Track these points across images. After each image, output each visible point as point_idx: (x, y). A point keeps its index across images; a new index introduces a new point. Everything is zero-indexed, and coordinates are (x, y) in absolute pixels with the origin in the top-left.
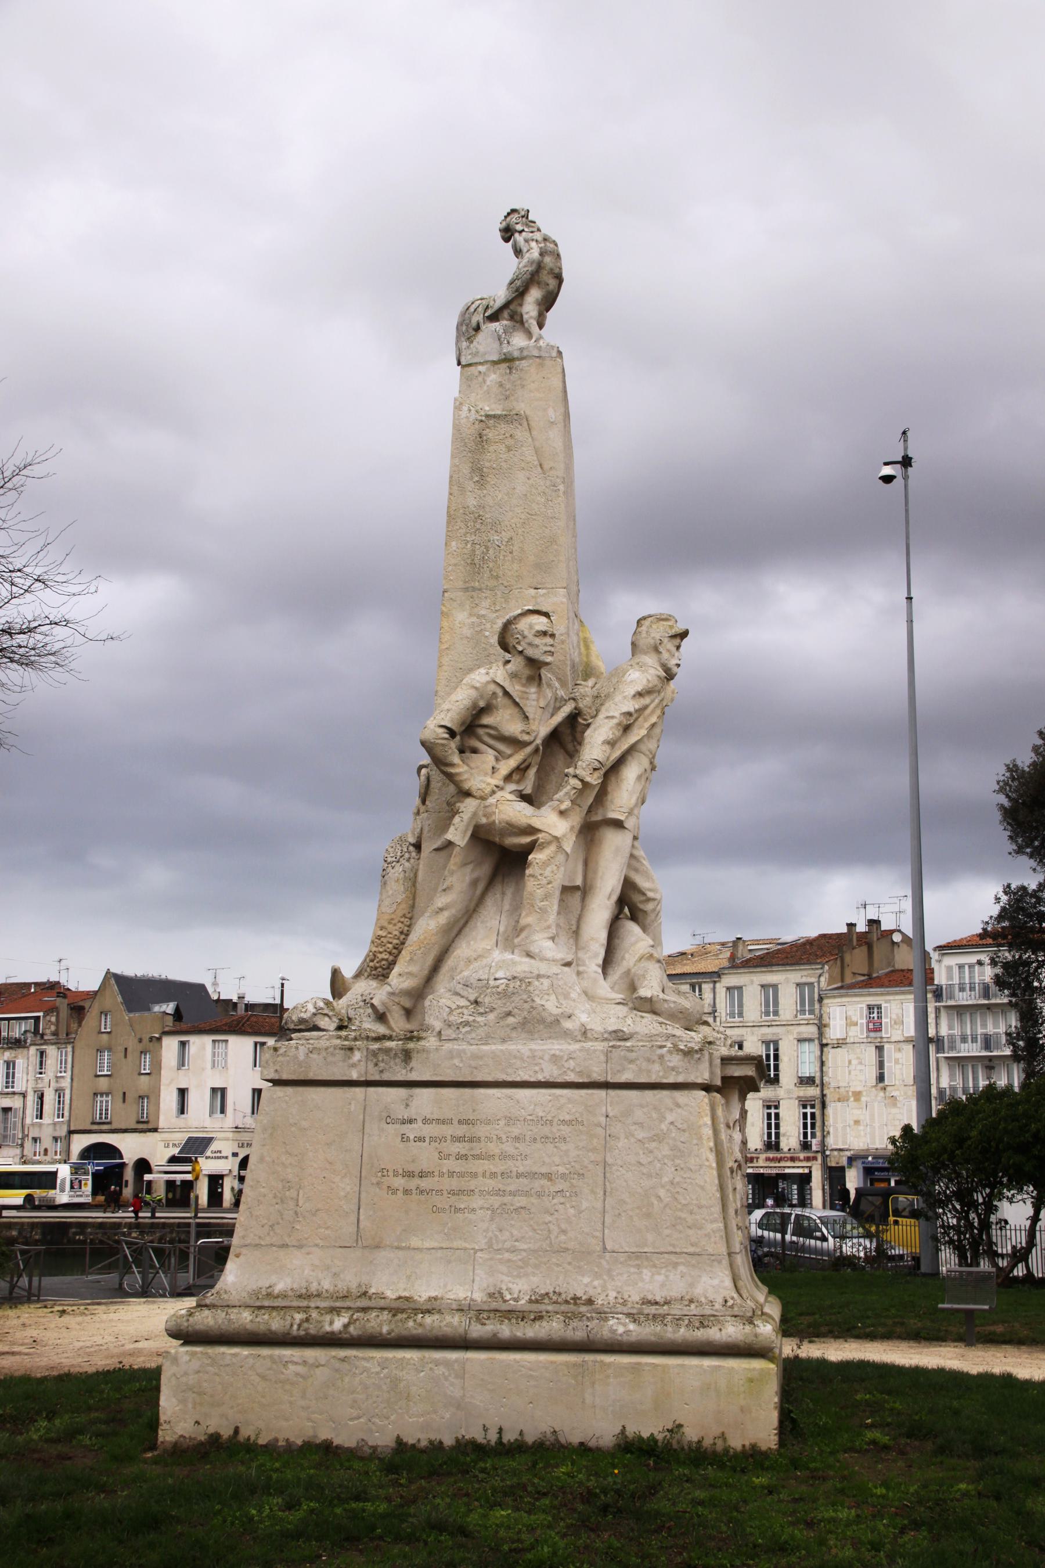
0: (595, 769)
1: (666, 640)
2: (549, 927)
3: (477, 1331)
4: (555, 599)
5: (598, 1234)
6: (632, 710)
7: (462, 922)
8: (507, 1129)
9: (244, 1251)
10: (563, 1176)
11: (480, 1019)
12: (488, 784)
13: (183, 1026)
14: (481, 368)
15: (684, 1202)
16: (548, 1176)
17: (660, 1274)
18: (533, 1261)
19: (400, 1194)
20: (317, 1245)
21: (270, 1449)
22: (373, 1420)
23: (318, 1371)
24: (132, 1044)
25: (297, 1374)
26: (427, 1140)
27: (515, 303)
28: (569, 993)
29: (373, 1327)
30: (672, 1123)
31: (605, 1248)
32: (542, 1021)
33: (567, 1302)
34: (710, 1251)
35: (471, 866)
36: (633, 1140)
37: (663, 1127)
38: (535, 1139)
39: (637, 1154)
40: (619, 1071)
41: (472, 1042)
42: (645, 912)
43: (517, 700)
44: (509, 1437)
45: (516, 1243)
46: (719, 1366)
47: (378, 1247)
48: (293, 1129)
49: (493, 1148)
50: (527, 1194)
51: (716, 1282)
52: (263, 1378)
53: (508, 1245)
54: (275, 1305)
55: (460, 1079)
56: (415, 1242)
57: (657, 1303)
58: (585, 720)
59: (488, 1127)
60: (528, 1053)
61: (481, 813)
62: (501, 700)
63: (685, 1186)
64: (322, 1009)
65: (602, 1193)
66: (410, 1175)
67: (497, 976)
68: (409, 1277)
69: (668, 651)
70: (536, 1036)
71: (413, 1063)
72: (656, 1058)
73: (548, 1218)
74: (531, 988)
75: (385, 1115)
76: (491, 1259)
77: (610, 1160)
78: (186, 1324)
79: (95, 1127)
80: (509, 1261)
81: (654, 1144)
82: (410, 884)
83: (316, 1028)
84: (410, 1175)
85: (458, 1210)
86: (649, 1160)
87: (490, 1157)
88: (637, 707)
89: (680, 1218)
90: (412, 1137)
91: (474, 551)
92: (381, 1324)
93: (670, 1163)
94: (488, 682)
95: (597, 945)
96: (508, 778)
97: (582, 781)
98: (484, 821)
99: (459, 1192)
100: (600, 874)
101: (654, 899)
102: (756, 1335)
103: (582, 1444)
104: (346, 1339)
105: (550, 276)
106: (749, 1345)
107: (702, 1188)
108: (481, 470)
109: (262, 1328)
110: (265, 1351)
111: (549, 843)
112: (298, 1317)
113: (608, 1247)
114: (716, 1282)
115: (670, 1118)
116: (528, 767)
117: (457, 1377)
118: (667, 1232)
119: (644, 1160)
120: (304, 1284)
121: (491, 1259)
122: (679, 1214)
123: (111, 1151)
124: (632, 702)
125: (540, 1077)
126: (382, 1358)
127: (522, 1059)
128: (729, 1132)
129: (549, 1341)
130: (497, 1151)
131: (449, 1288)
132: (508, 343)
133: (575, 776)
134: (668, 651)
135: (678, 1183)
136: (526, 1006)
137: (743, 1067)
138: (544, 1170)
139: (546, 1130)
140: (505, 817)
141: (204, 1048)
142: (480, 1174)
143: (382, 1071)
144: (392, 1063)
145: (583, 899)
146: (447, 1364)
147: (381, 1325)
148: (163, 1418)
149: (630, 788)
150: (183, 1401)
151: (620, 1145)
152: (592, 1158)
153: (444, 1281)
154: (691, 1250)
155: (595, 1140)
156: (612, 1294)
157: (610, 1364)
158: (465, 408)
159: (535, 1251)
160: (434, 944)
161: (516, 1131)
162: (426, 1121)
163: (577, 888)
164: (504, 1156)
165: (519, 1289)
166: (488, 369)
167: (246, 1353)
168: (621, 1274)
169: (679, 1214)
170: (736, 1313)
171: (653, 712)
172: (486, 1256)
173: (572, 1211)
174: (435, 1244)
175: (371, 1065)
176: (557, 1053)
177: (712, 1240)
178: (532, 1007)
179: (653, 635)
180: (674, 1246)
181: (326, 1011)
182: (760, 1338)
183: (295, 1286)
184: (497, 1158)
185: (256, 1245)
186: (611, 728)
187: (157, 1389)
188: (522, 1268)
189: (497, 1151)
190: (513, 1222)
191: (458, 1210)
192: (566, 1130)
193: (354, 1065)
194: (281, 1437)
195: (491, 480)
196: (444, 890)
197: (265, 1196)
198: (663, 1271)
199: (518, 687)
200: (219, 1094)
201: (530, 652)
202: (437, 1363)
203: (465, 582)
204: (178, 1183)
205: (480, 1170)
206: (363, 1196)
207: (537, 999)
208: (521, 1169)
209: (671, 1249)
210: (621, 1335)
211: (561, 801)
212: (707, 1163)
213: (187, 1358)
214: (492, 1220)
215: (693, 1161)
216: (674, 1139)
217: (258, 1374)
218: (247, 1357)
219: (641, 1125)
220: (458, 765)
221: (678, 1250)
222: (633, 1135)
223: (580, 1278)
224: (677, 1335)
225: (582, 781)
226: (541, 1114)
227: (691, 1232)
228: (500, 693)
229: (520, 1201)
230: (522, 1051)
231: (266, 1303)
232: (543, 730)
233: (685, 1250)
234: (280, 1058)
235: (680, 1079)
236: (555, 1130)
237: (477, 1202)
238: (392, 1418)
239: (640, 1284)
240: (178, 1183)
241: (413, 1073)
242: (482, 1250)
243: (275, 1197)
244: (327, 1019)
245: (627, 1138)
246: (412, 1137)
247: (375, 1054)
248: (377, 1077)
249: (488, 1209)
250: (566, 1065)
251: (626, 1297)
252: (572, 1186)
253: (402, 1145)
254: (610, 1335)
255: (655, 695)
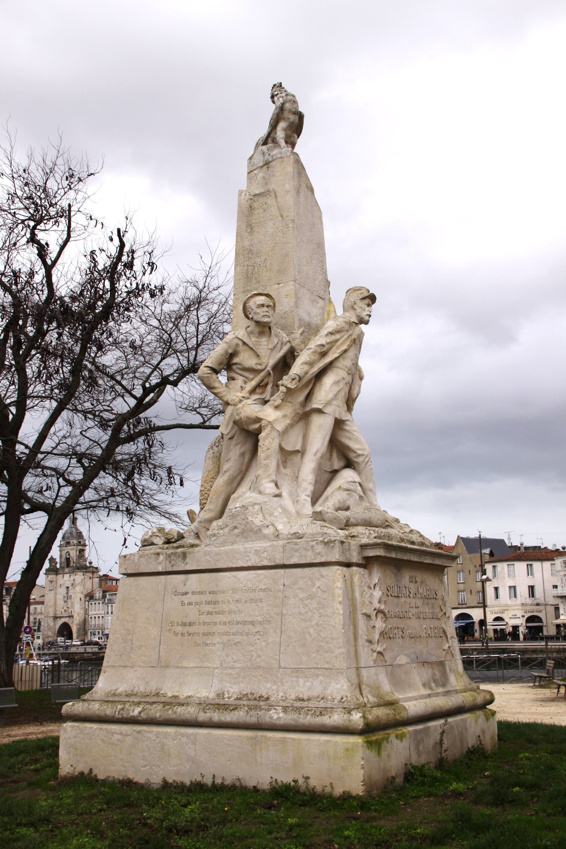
0: (293, 379)
1: (358, 302)
2: (270, 475)
3: (202, 717)
4: (288, 288)
5: (277, 657)
6: (324, 343)
7: (239, 478)
8: (233, 595)
9: (108, 669)
10: (260, 623)
11: (221, 532)
12: (237, 396)
13: (494, 559)
14: (256, 172)
15: (324, 636)
16: (252, 623)
17: (308, 681)
18: (242, 674)
19: (179, 635)
20: (140, 666)
21: (104, 782)
22: (153, 768)
23: (127, 738)
24: (472, 568)
25: (118, 740)
26: (194, 604)
27: (273, 133)
28: (273, 513)
29: (152, 714)
30: (319, 587)
31: (280, 666)
32: (252, 530)
33: (255, 699)
34: (337, 666)
35: (239, 446)
36: (297, 599)
37: (314, 590)
38: (246, 601)
39: (299, 607)
40: (290, 557)
41: (217, 545)
42: (358, 463)
43: (251, 346)
44: (218, 781)
45: (235, 664)
46: (329, 741)
47: (168, 667)
48: (132, 600)
49: (225, 607)
50: (241, 634)
51: (339, 686)
52: (103, 741)
53: (230, 665)
54: (115, 700)
55: (210, 568)
56: (185, 664)
57: (303, 700)
58: (298, 353)
59: (223, 595)
60: (243, 550)
61: (235, 414)
62: (241, 347)
63: (324, 626)
64: (154, 533)
65: (280, 632)
66: (184, 624)
67: (236, 506)
68: (181, 684)
69: (360, 307)
70: (249, 539)
71: (188, 560)
72: (309, 548)
73: (252, 648)
74: (247, 512)
75: (174, 590)
76: (222, 673)
77: (284, 612)
78: (70, 710)
79: (460, 606)
80: (231, 674)
81: (309, 601)
82: (216, 459)
83: (153, 544)
84: (184, 624)
85: (207, 645)
86: (306, 610)
87: (223, 613)
88: (328, 341)
89: (321, 646)
90: (186, 603)
91: (248, 270)
92: (156, 712)
93: (317, 612)
94: (234, 338)
95: (306, 484)
96: (253, 391)
97: (286, 387)
98: (237, 418)
99: (209, 634)
100: (309, 441)
101: (363, 455)
102: (350, 721)
103: (254, 787)
104: (141, 720)
105: (290, 114)
106: (346, 727)
107: (334, 627)
108: (251, 225)
109: (102, 713)
110: (105, 726)
111: (267, 426)
112: (120, 707)
113: (282, 665)
114: (339, 686)
115: (318, 584)
116: (267, 384)
117: (192, 744)
118: (314, 655)
119: (303, 611)
120: (132, 688)
121: (222, 673)
122: (321, 644)
123: (468, 616)
124: (325, 339)
125: (249, 564)
126: (156, 731)
127: (240, 553)
128: (371, 591)
129: (238, 723)
130: (227, 609)
131: (199, 691)
132: (269, 155)
133: (282, 385)
134: (360, 307)
135: (321, 624)
136: (244, 522)
137: (374, 550)
138: (250, 619)
139: (252, 595)
140: (246, 414)
141: (503, 568)
142: (218, 623)
143: (173, 566)
144: (177, 561)
145: (302, 457)
146: (188, 736)
147: (156, 713)
148: (61, 762)
149: (327, 389)
150: (69, 753)
151: (290, 602)
152: (275, 611)
153: (194, 687)
154: (326, 666)
155: (277, 600)
156: (281, 694)
157: (269, 738)
158: (243, 194)
159: (244, 668)
160: (222, 492)
161: (237, 597)
162: (193, 593)
163: (298, 451)
164: (230, 612)
165: (233, 690)
166: (259, 171)
167: (95, 727)
168: (287, 682)
169: (321, 644)
170: (345, 706)
171: (343, 343)
172: (219, 672)
173: (264, 643)
174: (195, 665)
175: (168, 562)
176: (258, 548)
177: (339, 660)
178: (247, 523)
179: (350, 300)
180: (317, 664)
181: (157, 534)
182: (353, 723)
183: (128, 689)
184: (227, 613)
185: (113, 666)
186: (308, 355)
187: (58, 747)
188: (237, 678)
189: (227, 609)
190: (233, 651)
191: (207, 645)
192: (262, 594)
193: (160, 563)
194: (112, 775)
195: (256, 229)
196: (227, 461)
197: (118, 638)
198: (310, 680)
199: (253, 339)
200: (513, 589)
201: (256, 318)
202: (183, 735)
203: (244, 288)
204: (499, 630)
205: (218, 621)
206: (162, 637)
207: (250, 518)
208: (239, 619)
209: (315, 666)
210: (275, 720)
211: (275, 401)
212: (337, 611)
213: (70, 729)
214: (223, 650)
215: (329, 611)
216: (319, 597)
217: (101, 739)
218: (96, 729)
219: (301, 589)
220: (219, 388)
221: (319, 666)
222: (297, 596)
223: (266, 684)
224: (305, 721)
225: (286, 387)
226: (250, 586)
227: (327, 655)
228: (240, 343)
229: (238, 638)
230: (240, 549)
231: (111, 699)
232: (272, 362)
233: (323, 667)
234: (127, 562)
235: (323, 560)
236: (257, 595)
237: (216, 639)
238: (162, 767)
239: (297, 688)
240: (499, 630)
241: (188, 565)
242: (217, 668)
243: (123, 639)
244: (158, 538)
245: (294, 598)
246: (186, 603)
247: (169, 556)
248: (170, 569)
249: (221, 643)
250: (263, 555)
251: (288, 696)
252: (264, 628)
253: (181, 608)
254: (269, 720)
255: (343, 333)
